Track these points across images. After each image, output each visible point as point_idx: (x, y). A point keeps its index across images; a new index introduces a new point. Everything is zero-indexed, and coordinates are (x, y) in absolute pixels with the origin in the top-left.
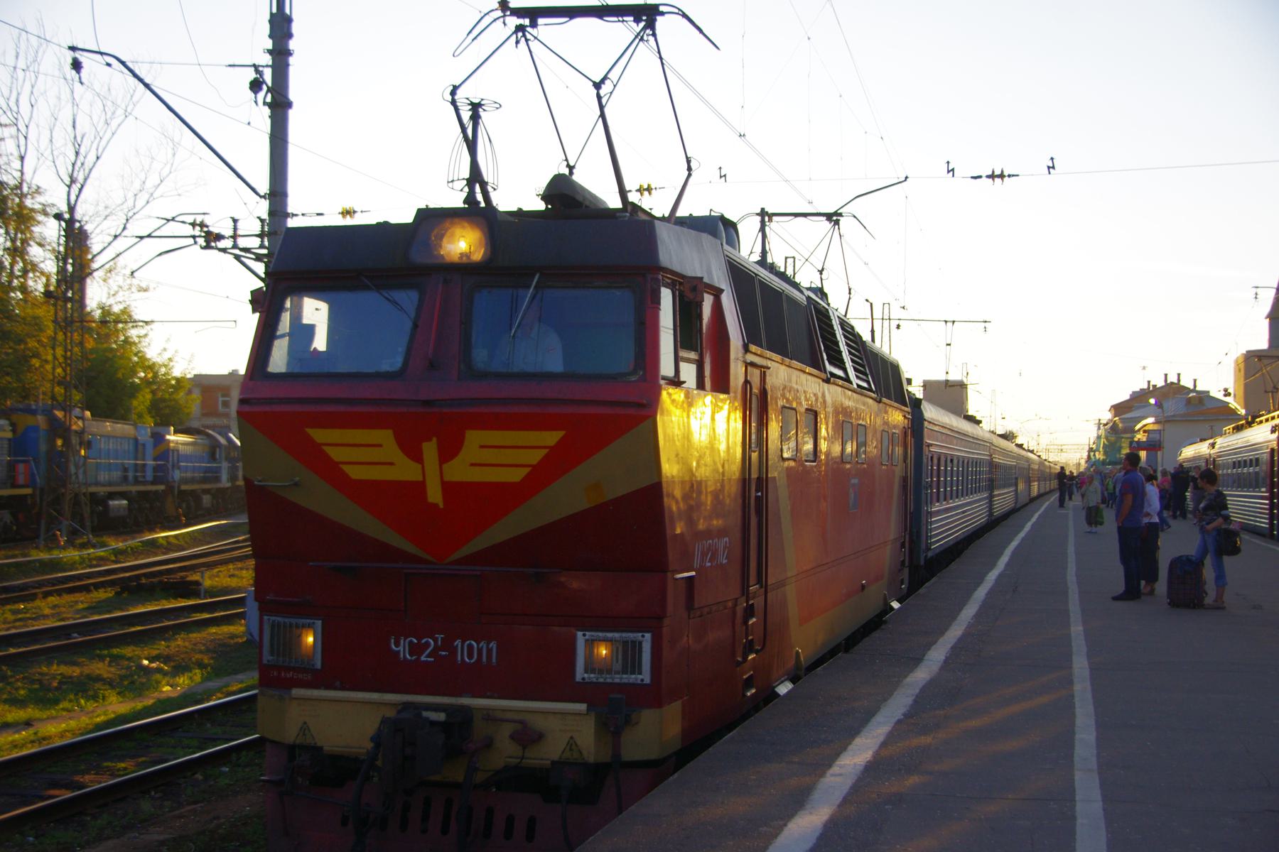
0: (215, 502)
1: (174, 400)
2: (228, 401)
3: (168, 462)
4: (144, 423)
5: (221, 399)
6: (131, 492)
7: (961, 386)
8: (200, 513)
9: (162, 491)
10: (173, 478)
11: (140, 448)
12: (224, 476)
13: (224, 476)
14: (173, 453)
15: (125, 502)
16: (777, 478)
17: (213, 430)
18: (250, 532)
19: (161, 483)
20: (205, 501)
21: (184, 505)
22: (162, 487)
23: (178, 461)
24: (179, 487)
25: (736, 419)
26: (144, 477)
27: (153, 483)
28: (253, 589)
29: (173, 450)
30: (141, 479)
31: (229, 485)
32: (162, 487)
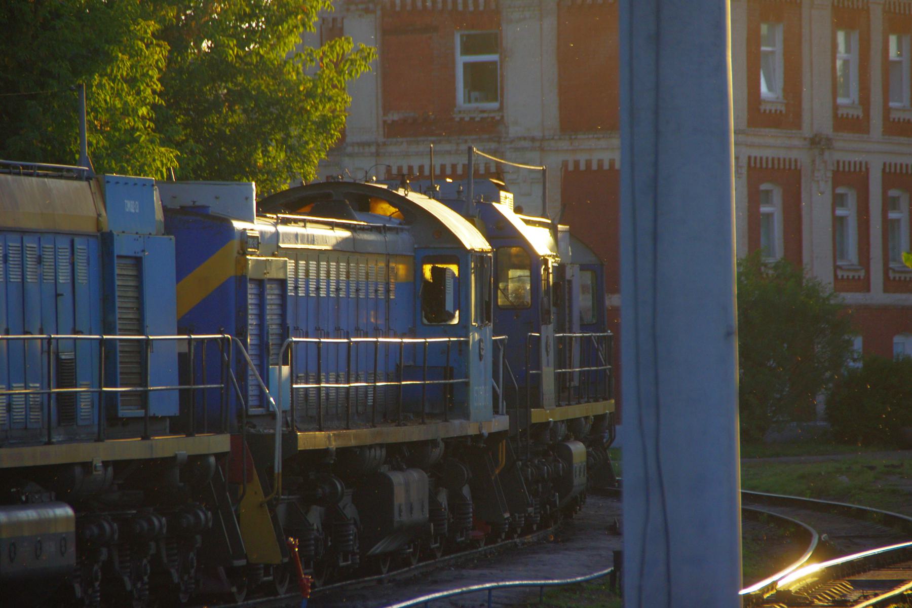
0: (443, 498)
1: (262, 66)
2: (494, 63)
3: (241, 333)
4: (141, 170)
5: (461, 60)
6: (87, 466)
7: (581, 270)
8: (379, 548)
9: (219, 456)
10: (262, 399)
11: (122, 272)
12: (282, 497)
13: (282, 497)
14: (261, 296)
15: (66, 511)
16: (260, 238)
17: (430, 192)
18: (614, 566)
19: (216, 428)
20: (399, 498)
21: (315, 516)
22: (220, 443)
23: (284, 333)
24: (290, 439)
25: (296, 288)
26: (143, 399)
27: (178, 426)
28: (763, 48)
29: (260, 283)
30: (124, 412)
31: (501, 423)
32: (220, 443)
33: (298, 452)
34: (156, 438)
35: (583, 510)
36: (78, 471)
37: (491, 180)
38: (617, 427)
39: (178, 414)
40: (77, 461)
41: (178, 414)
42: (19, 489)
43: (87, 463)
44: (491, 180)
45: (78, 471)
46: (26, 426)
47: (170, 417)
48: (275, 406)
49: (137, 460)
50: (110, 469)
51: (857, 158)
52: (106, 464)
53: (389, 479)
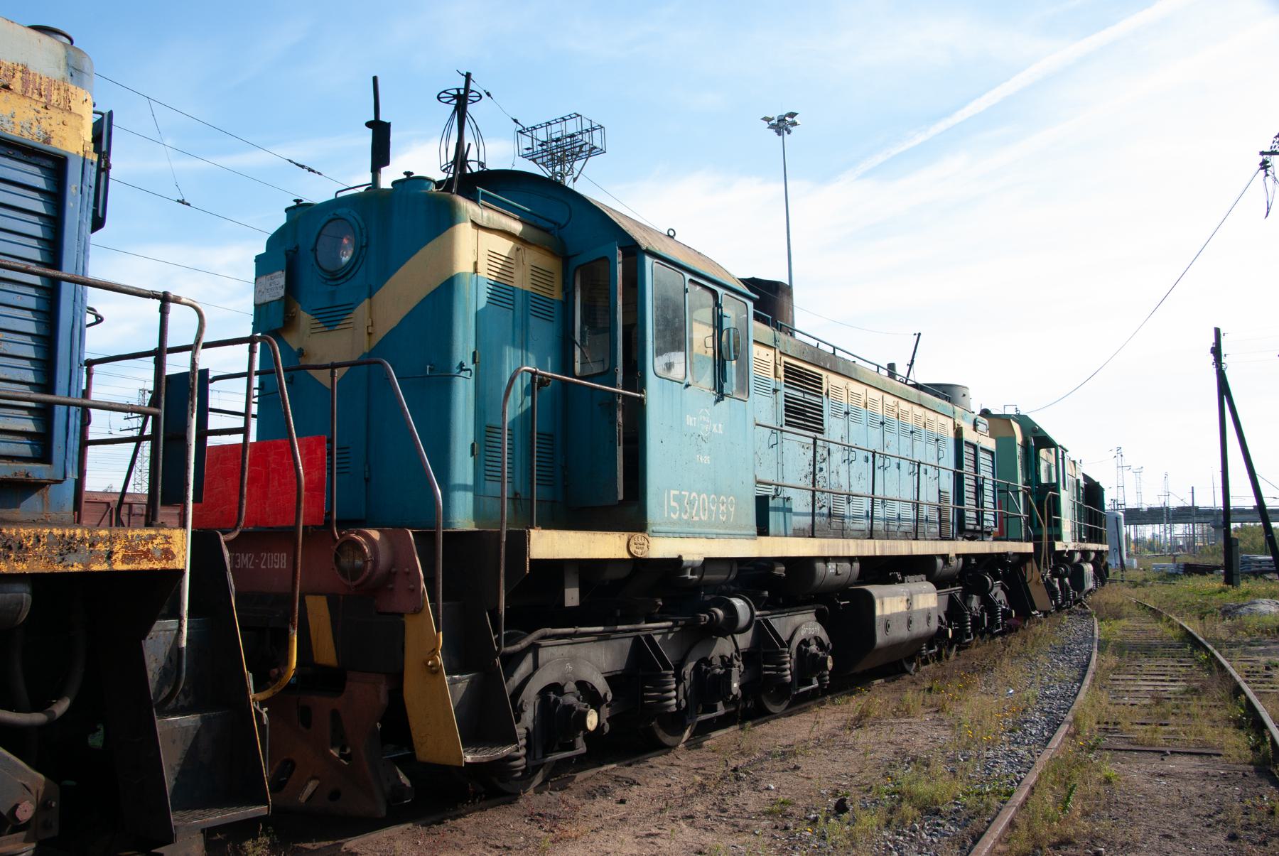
6: (945, 558)
33: (617, 503)
34: (309, 846)
35: (1121, 601)
36: (940, 562)
37: (153, 851)
38: (77, 477)
39: (566, 605)
40: (939, 553)
41: (566, 605)
42: (30, 531)
43: (945, 555)
44: (153, 851)
45: (940, 562)
46: (837, 572)
47: (414, 754)
48: (185, 653)
49: (588, 769)
50: (961, 560)
51: (766, 493)
52: (958, 556)
53: (1082, 567)
